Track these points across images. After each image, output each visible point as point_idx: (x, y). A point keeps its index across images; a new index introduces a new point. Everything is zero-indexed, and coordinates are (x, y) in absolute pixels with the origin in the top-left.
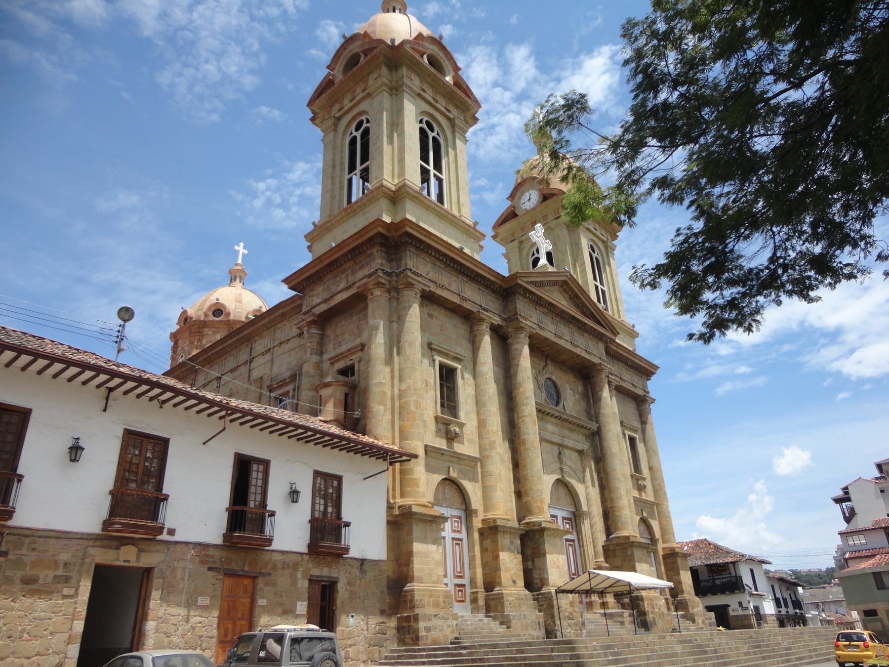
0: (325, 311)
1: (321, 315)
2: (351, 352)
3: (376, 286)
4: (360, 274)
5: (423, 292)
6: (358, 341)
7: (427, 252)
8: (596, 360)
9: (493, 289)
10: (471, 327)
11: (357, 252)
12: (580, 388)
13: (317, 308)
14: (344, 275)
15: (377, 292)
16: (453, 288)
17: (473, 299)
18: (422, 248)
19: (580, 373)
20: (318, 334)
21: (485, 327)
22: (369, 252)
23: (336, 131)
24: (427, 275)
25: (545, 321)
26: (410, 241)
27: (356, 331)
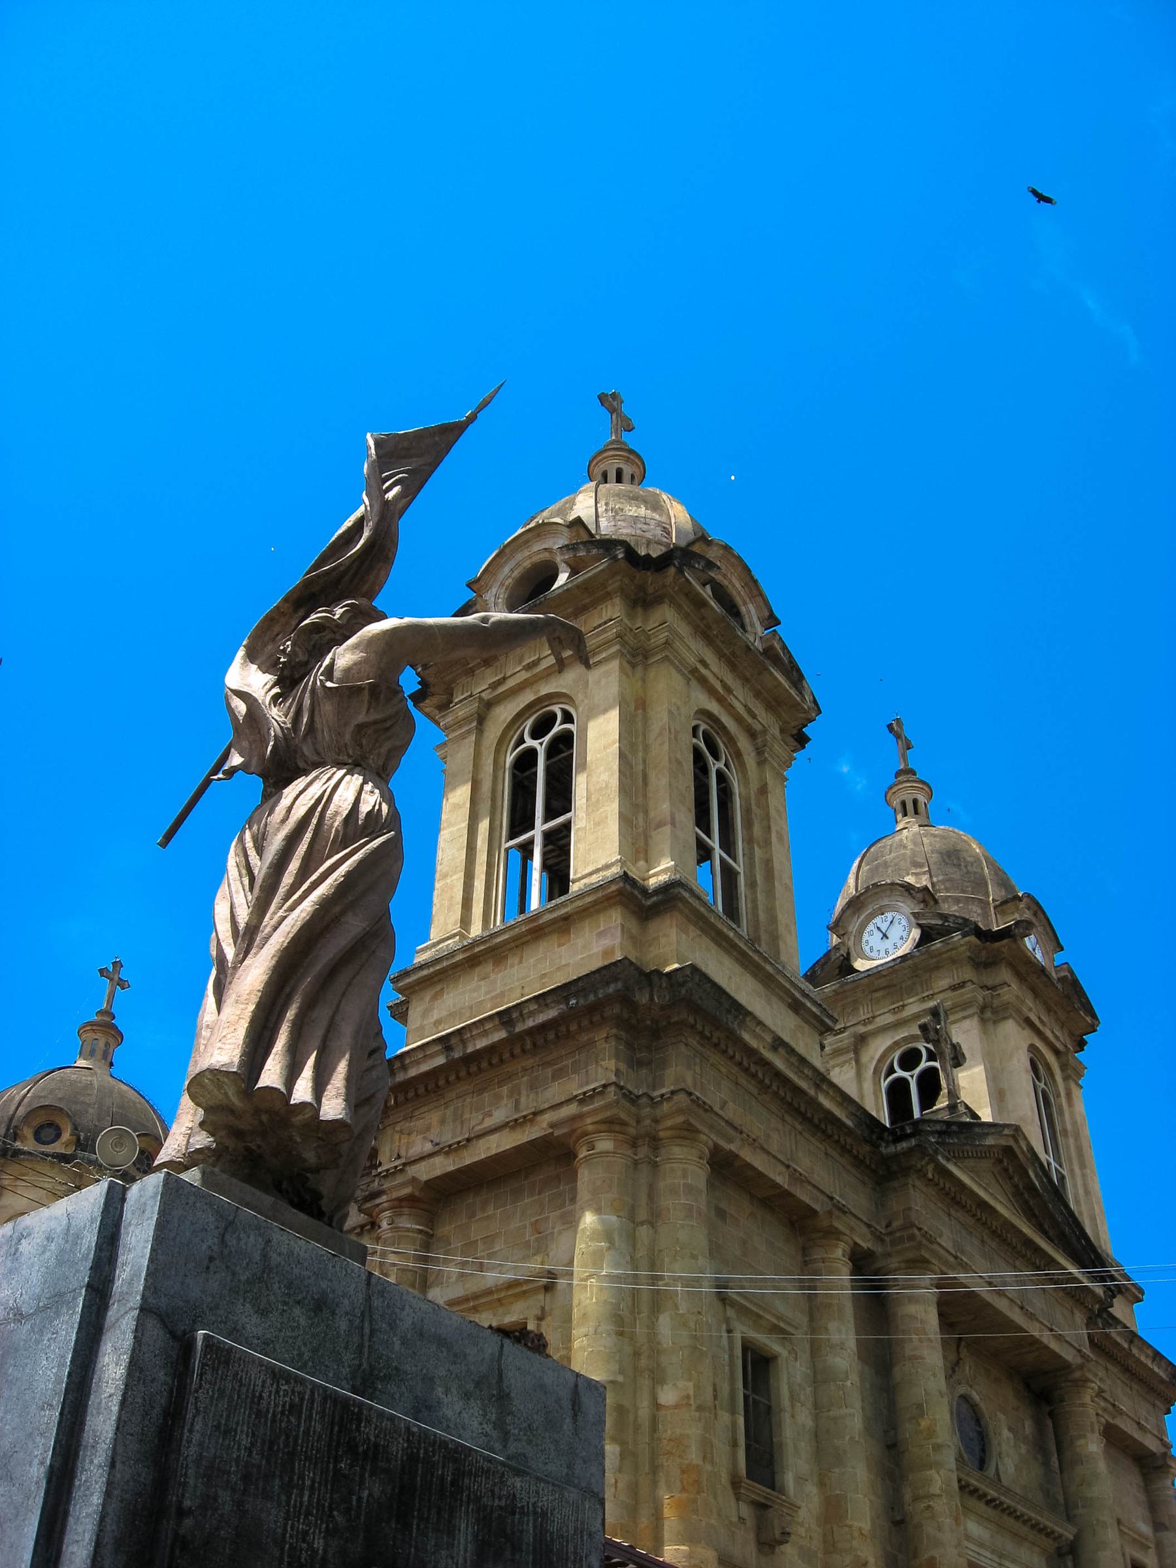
0: (448, 1175)
1: (430, 1184)
2: (515, 1289)
3: (603, 1127)
4: (556, 1091)
5: (716, 1150)
6: (535, 1265)
7: (725, 1052)
8: (1068, 1355)
9: (856, 1157)
10: (805, 1251)
11: (551, 1036)
12: (1028, 1427)
13: (423, 1165)
14: (505, 1090)
15: (605, 1144)
16: (774, 1148)
17: (815, 1179)
18: (715, 1040)
19: (1027, 1386)
20: (420, 1231)
21: (839, 1252)
22: (584, 1038)
23: (480, 730)
24: (722, 1108)
25: (968, 1248)
26: (691, 1020)
27: (529, 1236)
